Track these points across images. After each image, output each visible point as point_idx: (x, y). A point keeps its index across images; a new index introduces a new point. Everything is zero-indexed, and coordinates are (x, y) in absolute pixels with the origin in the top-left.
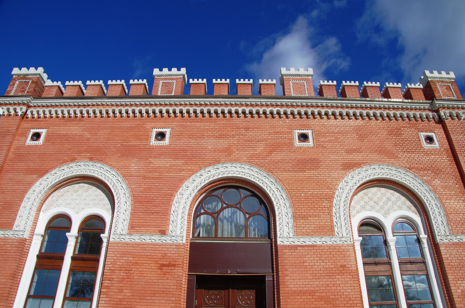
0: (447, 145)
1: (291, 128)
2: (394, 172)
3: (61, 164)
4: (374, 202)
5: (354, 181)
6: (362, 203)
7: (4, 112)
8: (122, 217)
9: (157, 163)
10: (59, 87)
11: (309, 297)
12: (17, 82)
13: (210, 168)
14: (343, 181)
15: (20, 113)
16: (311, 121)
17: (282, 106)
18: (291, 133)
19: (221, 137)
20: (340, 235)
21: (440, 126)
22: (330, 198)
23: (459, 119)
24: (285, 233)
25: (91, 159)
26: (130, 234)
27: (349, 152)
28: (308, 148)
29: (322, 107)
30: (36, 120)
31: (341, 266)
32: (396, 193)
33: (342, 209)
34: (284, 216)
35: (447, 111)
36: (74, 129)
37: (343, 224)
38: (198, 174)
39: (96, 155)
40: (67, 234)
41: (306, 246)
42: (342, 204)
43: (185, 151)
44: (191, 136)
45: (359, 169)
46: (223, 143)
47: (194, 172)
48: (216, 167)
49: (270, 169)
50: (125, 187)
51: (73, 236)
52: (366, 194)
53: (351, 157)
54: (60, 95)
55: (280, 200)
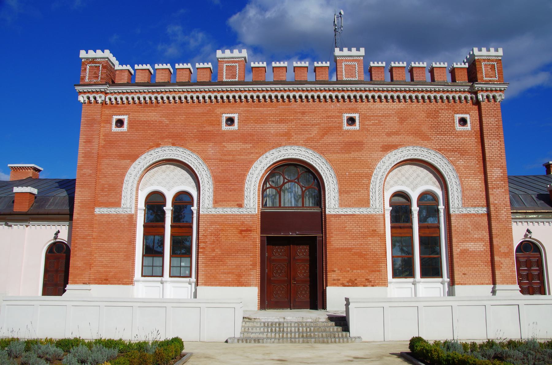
0: (478, 128)
1: (341, 112)
2: (425, 153)
3: (148, 149)
4: (406, 178)
5: (390, 162)
6: (396, 179)
7: (84, 101)
8: (207, 194)
9: (231, 147)
10: (129, 70)
11: (348, 252)
12: (88, 67)
13: (274, 151)
14: (381, 161)
15: (100, 101)
16: (360, 105)
17: (334, 91)
18: (341, 117)
19: (281, 121)
20: (374, 207)
21: (476, 107)
22: (369, 176)
23: (495, 101)
24: (332, 204)
25: (174, 144)
26: (215, 207)
27: (389, 134)
28: (354, 131)
29: (370, 91)
30: (115, 106)
31: (373, 230)
32: (425, 170)
33: (377, 185)
34: (332, 191)
35: (485, 94)
36: (153, 115)
37: (377, 198)
38: (264, 156)
39: (177, 140)
40: (164, 208)
41: (347, 215)
42: (378, 181)
43: (251, 135)
44: (257, 121)
45: (396, 151)
46: (283, 128)
47: (260, 154)
48: (278, 150)
49: (322, 151)
50: (206, 169)
51: (168, 208)
52: (400, 171)
53: (390, 139)
54: (132, 82)
55: (329, 178)
